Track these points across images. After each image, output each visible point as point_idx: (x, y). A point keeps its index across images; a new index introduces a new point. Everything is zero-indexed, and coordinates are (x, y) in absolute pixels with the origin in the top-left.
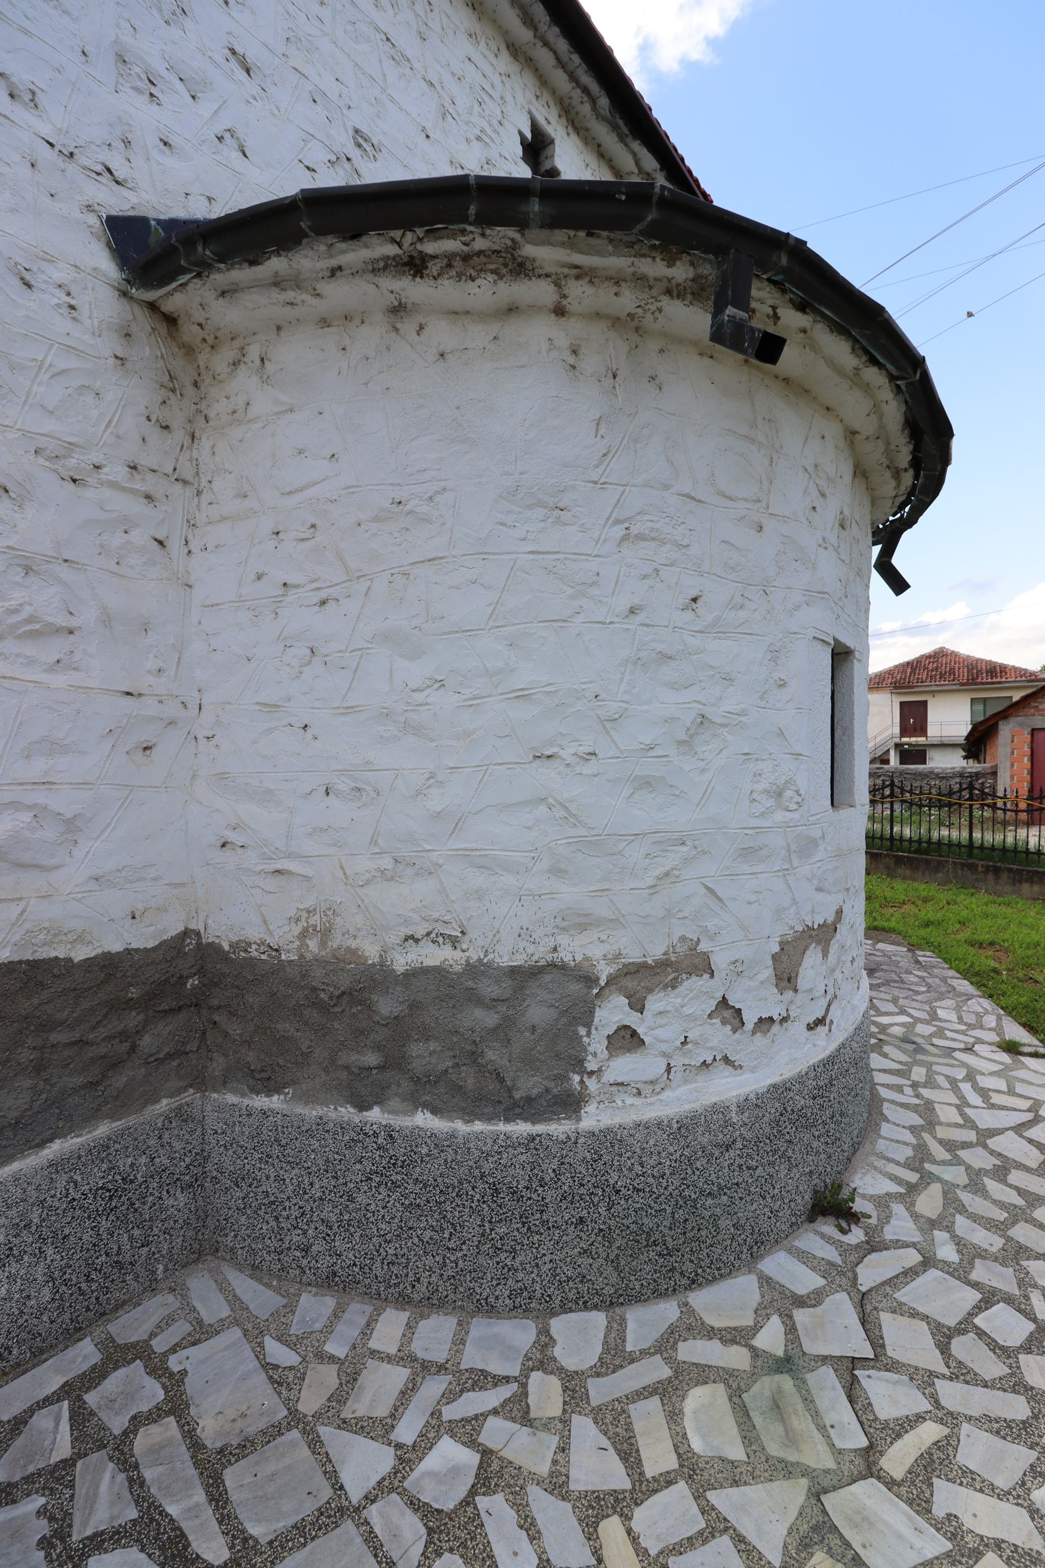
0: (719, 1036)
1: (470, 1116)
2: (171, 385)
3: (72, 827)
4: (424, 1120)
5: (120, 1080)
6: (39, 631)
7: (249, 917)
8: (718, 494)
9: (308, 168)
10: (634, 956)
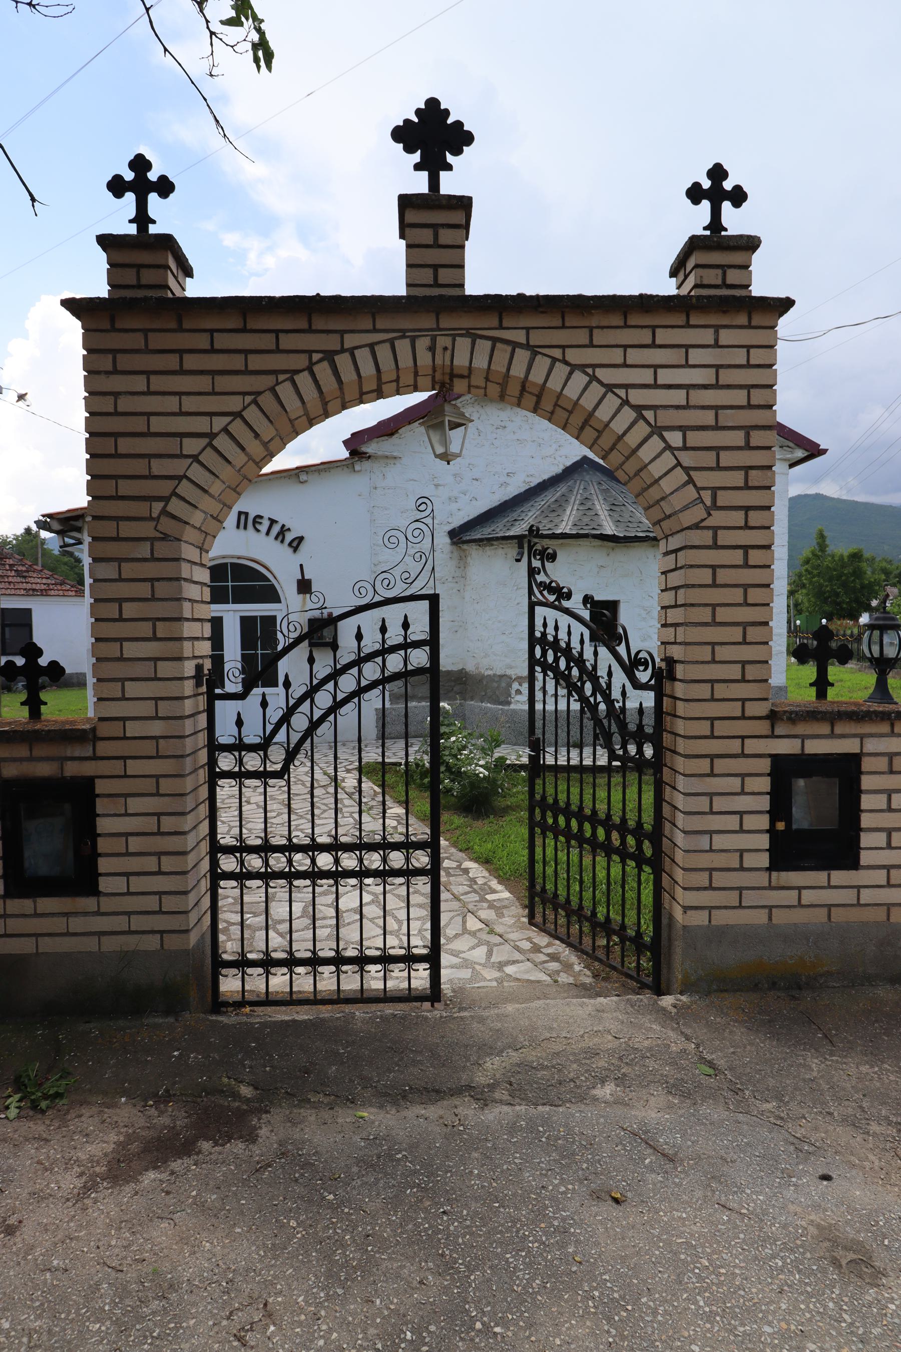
2: (461, 558)
4: (489, 705)
7: (470, 668)
8: (791, 466)
10: (520, 675)
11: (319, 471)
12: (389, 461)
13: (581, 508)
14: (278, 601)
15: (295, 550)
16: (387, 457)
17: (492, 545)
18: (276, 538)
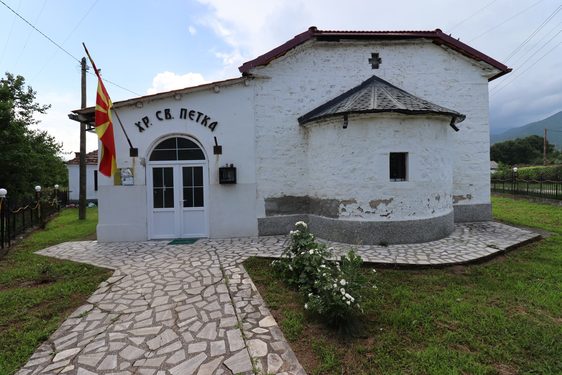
0: (359, 212)
1: (328, 217)
2: (305, 134)
3: (295, 183)
4: (324, 217)
5: (300, 210)
6: (292, 163)
7: (311, 195)
8: (490, 80)
9: (176, 242)
10: (345, 199)
11: (226, 86)
12: (264, 80)
13: (379, 98)
14: (203, 158)
15: (213, 130)
16: (263, 78)
17: (326, 121)
18: (202, 123)
